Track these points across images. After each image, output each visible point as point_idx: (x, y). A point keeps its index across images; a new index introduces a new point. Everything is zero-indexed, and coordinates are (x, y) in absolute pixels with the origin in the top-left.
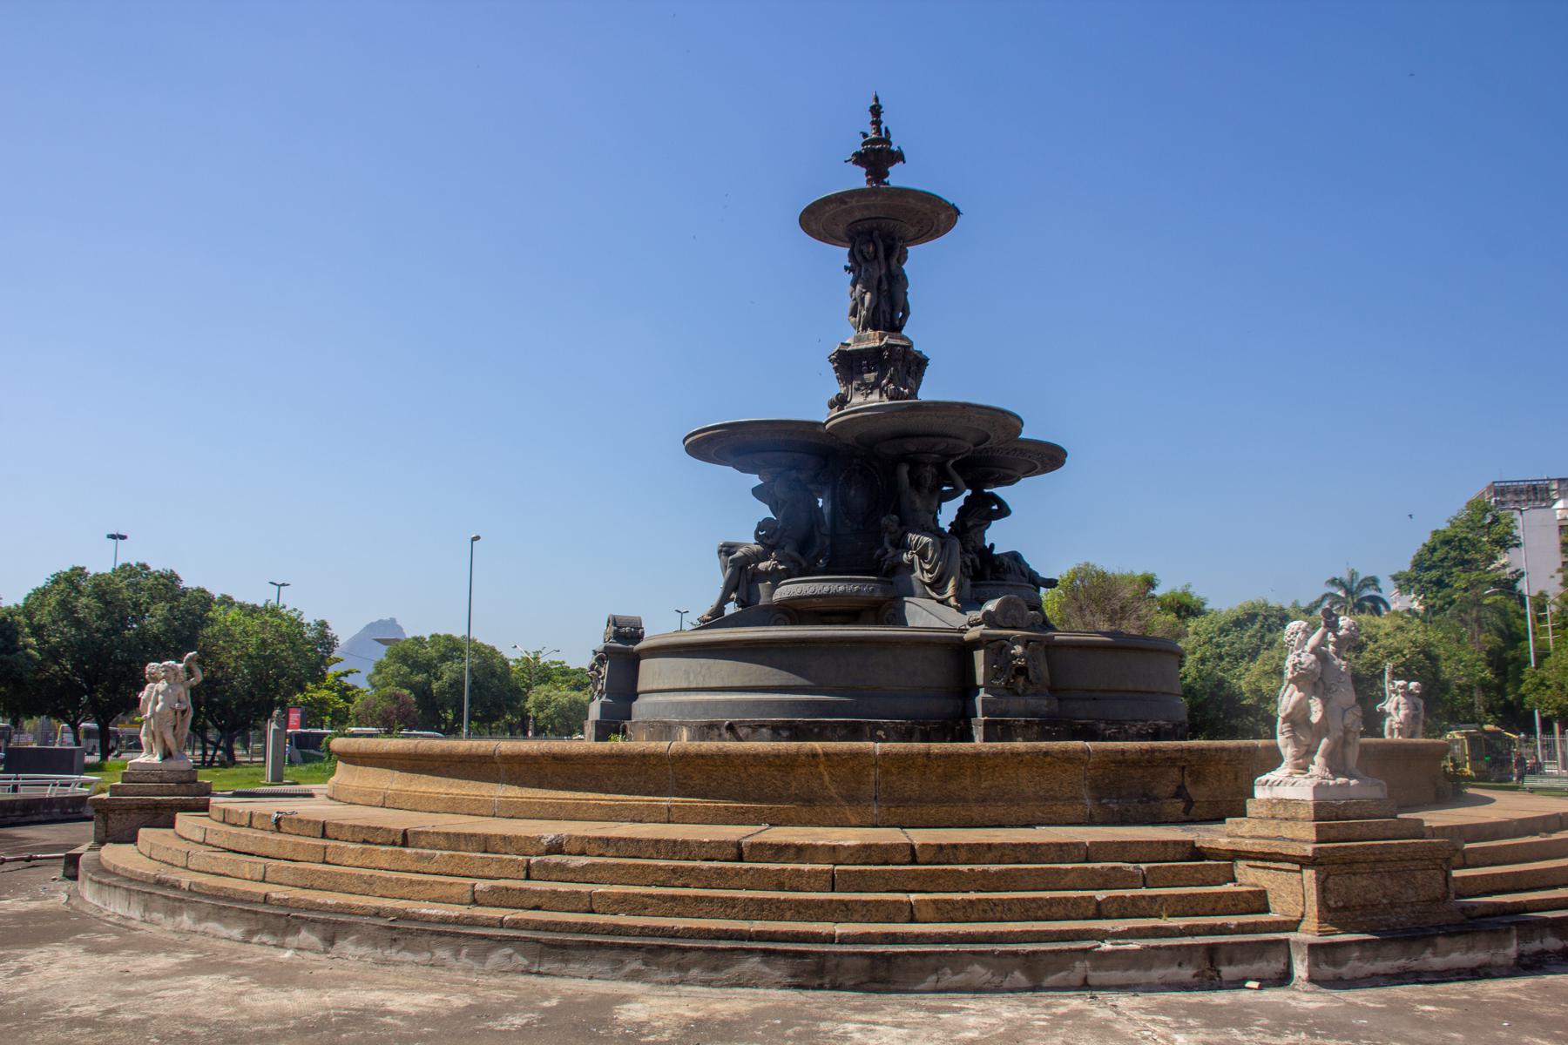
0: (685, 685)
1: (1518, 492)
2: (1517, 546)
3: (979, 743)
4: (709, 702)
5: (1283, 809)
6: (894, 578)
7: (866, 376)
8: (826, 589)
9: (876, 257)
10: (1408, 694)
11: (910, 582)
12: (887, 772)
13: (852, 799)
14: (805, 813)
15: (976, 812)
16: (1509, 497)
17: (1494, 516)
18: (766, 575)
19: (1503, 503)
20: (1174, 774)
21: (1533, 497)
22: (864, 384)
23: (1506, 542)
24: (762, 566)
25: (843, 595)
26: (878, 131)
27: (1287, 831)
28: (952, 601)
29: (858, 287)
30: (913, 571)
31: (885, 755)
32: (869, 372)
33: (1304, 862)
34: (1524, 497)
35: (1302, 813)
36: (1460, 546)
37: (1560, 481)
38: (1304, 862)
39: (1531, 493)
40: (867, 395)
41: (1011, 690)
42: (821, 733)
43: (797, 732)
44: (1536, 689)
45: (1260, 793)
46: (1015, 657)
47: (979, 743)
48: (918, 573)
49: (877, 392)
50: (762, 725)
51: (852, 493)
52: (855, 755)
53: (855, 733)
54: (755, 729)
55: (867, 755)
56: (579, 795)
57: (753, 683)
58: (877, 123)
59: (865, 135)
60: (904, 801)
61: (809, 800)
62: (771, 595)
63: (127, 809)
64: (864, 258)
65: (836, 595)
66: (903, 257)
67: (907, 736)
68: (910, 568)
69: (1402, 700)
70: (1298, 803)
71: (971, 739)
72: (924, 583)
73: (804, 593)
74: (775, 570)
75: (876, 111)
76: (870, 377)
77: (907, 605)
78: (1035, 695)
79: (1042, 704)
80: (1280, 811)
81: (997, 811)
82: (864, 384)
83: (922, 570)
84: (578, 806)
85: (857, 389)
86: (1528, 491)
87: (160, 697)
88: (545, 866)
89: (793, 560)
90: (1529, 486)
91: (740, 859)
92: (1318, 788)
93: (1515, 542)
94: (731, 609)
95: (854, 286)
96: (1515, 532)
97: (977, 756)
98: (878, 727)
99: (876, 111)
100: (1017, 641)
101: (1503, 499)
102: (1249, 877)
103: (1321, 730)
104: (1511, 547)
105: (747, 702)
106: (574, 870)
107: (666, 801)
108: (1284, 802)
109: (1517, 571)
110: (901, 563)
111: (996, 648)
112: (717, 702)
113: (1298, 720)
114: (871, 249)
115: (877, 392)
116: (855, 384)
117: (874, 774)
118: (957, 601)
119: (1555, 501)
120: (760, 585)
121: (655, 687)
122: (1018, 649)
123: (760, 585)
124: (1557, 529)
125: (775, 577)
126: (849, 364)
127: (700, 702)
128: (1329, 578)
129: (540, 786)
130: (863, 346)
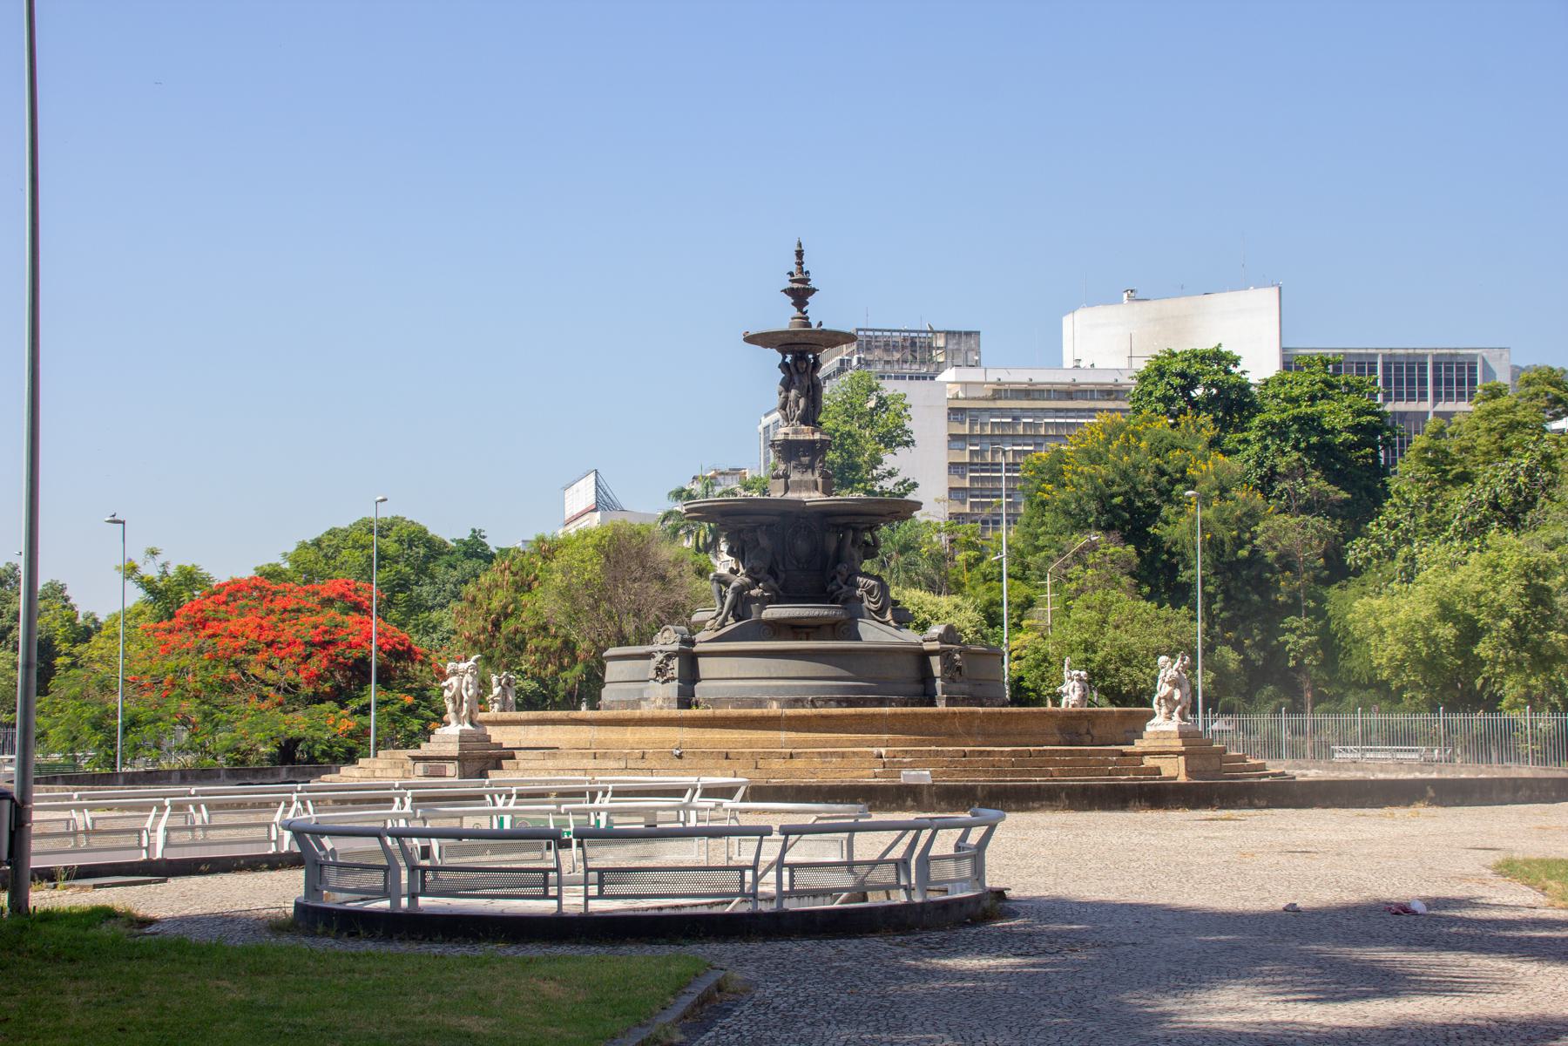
0: (768, 676)
1: (888, 347)
2: (907, 444)
3: (941, 707)
4: (790, 686)
5: (1165, 735)
6: (854, 610)
7: (802, 459)
8: (817, 613)
9: (806, 371)
10: (1080, 680)
11: (861, 608)
12: (982, 721)
13: (969, 734)
14: (951, 741)
15: (1018, 739)
16: (877, 353)
17: (880, 398)
18: (755, 599)
19: (868, 364)
20: (1086, 723)
21: (910, 358)
22: (801, 464)
23: (895, 438)
24: (753, 592)
25: (827, 616)
26: (801, 271)
27: (1167, 743)
28: (892, 623)
29: (793, 393)
30: (862, 601)
31: (984, 713)
32: (805, 456)
33: (1179, 754)
34: (897, 356)
35: (1173, 736)
36: (842, 445)
37: (949, 334)
38: (1179, 754)
39: (908, 352)
40: (803, 472)
41: (953, 680)
42: (865, 703)
43: (851, 703)
44: (1038, 666)
45: (1149, 729)
46: (956, 660)
47: (941, 707)
48: (866, 603)
49: (810, 470)
50: (830, 700)
51: (799, 542)
52: (972, 713)
53: (881, 703)
54: (827, 702)
55: (977, 713)
56: (836, 735)
57: (819, 675)
58: (800, 264)
59: (791, 274)
60: (989, 735)
61: (952, 735)
62: (761, 613)
63: (474, 759)
64: (797, 370)
65: (823, 617)
66: (779, 351)
67: (906, 705)
68: (861, 600)
69: (1077, 684)
70: (1171, 732)
71: (1045, 705)
72: (870, 610)
73: (801, 615)
74: (763, 596)
75: (800, 254)
76: (806, 460)
77: (860, 624)
78: (962, 682)
79: (965, 687)
80: (1161, 735)
81: (1026, 739)
82: (801, 464)
83: (869, 601)
84: (837, 741)
85: (794, 467)
86: (903, 347)
87: (470, 686)
88: (893, 762)
89: (777, 593)
90: (905, 339)
91: (965, 756)
92: (1180, 726)
93: (906, 438)
94: (732, 624)
95: (788, 390)
96: (908, 425)
97: (942, 717)
98: (892, 700)
99: (800, 254)
100: (956, 651)
101: (869, 357)
102: (1149, 762)
103: (1179, 702)
104: (899, 445)
105: (817, 686)
106: (906, 763)
107: (886, 737)
108: (1164, 732)
109: (905, 481)
110: (854, 596)
111: (945, 655)
112: (795, 686)
113: (1169, 699)
114: (805, 366)
115: (810, 470)
116: (793, 463)
117: (977, 722)
118: (896, 622)
119: (940, 367)
120: (752, 606)
121: (734, 676)
122: (957, 656)
123: (752, 606)
124: (946, 412)
125: (765, 602)
126: (789, 450)
127: (783, 686)
128: (674, 488)
129: (809, 731)
130: (801, 437)
